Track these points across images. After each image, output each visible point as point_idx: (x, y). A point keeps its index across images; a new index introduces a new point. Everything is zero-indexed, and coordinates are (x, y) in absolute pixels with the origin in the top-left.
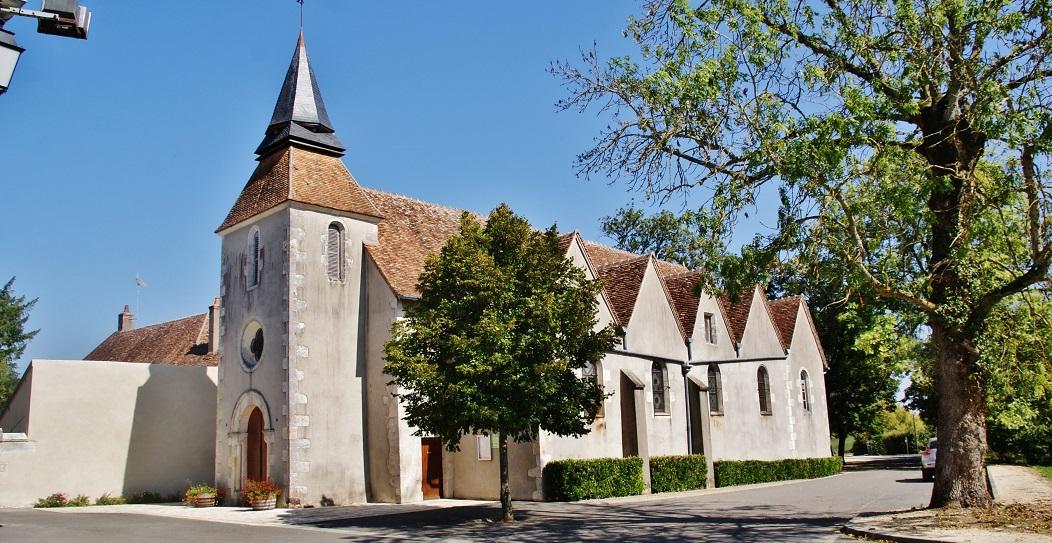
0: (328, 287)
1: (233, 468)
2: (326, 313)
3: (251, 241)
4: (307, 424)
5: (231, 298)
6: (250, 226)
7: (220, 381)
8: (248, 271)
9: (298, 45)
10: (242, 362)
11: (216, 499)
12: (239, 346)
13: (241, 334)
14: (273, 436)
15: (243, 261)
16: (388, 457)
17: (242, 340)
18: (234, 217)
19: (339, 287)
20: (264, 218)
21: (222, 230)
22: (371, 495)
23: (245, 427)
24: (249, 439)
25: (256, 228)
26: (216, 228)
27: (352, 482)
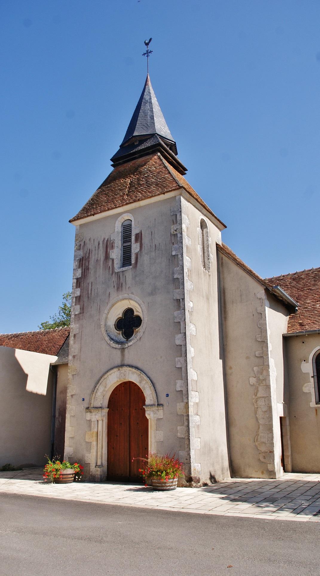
0: (203, 274)
1: (94, 443)
2: (203, 297)
3: (118, 228)
4: (197, 401)
5: (91, 278)
6: (120, 214)
7: (262, 315)
8: (116, 254)
9: (146, 84)
10: (107, 338)
11: (76, 474)
12: (103, 323)
13: (106, 312)
14: (100, 415)
15: (108, 245)
16: (258, 435)
17: (107, 318)
18: (89, 209)
19: (208, 275)
20: (140, 207)
21: (78, 219)
22: (234, 472)
23: (106, 403)
24: (109, 414)
25: (126, 217)
26: (71, 218)
27: (222, 456)
